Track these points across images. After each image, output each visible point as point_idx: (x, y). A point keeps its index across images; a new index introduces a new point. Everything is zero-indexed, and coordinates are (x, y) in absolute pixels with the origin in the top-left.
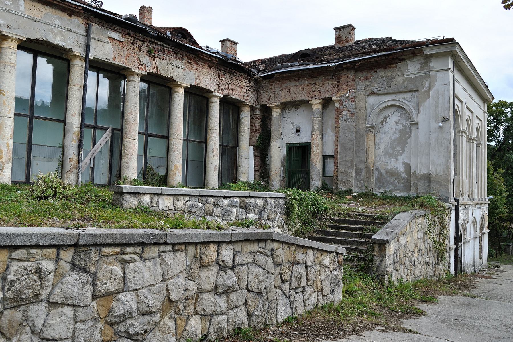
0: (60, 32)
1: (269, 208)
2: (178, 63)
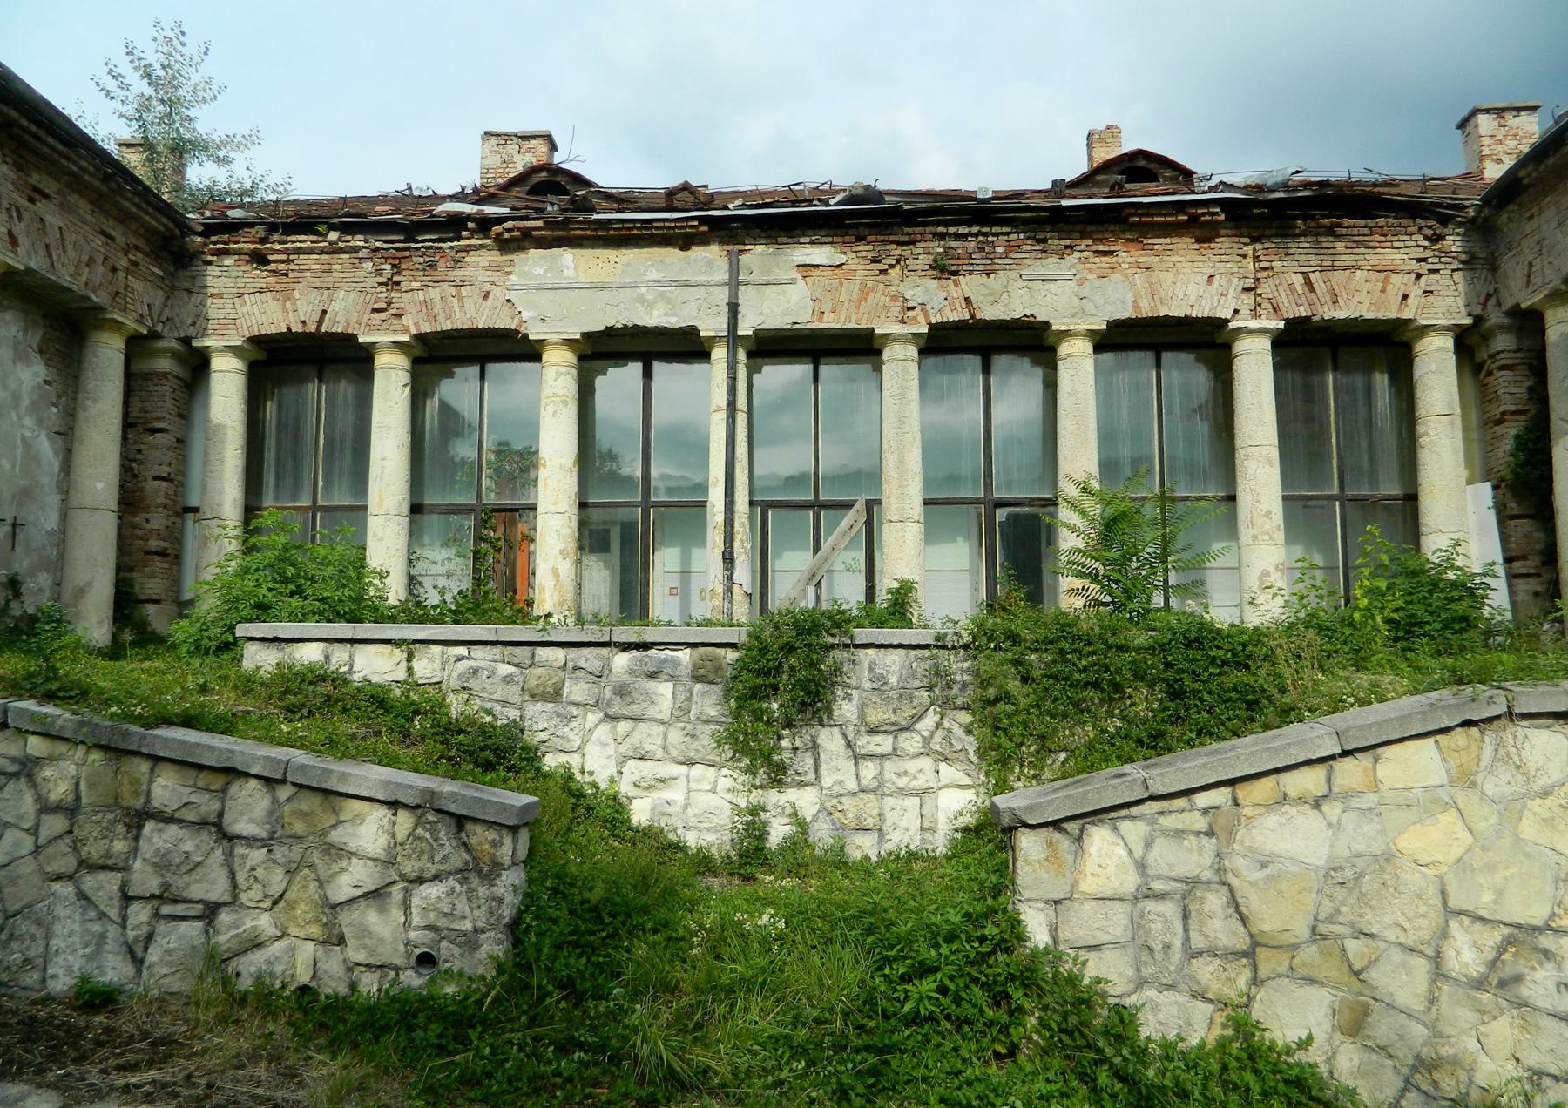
0: (662, 295)
1: (867, 685)
2: (1051, 266)
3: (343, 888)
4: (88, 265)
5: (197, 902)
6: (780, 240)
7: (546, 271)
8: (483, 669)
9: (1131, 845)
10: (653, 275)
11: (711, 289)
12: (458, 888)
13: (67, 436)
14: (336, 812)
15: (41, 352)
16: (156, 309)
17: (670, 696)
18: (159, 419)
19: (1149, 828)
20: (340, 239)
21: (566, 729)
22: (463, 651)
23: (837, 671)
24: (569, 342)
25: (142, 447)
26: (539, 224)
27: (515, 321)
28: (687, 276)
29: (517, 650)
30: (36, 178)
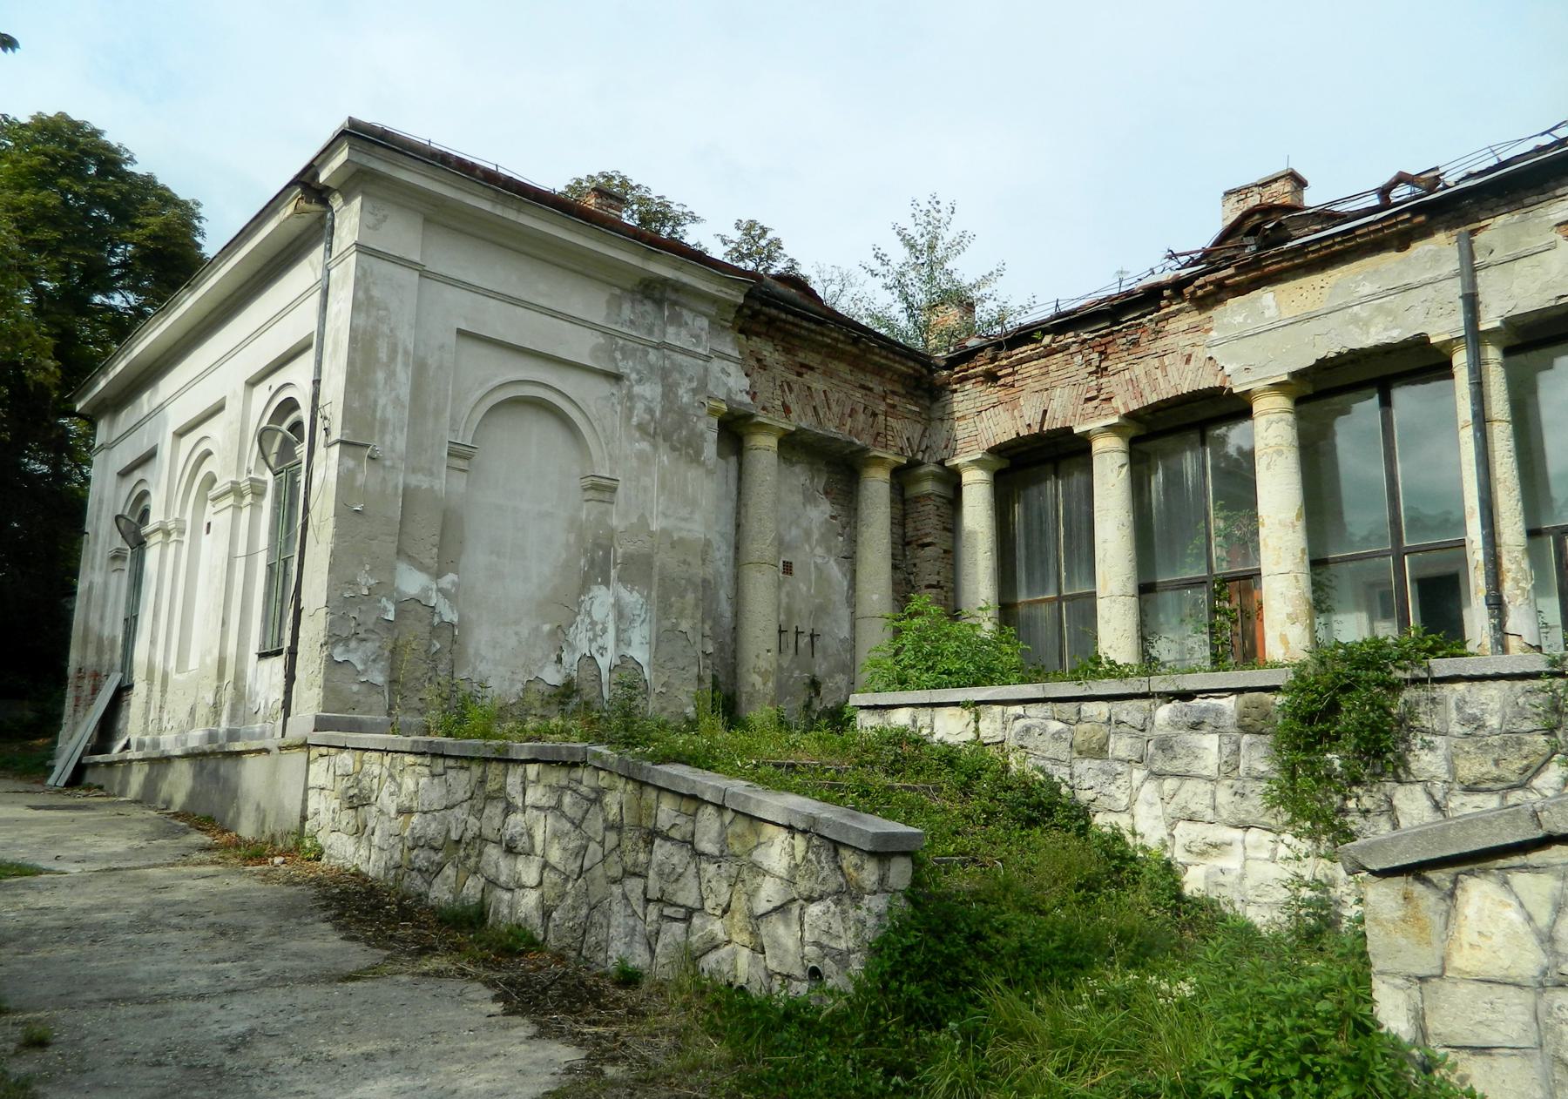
1: (1457, 729)
3: (762, 906)
4: (850, 416)
5: (682, 906)
6: (1527, 201)
7: (1246, 318)
8: (1035, 726)
9: (1530, 908)
10: (1367, 289)
11: (1440, 285)
12: (833, 908)
13: (850, 559)
14: (758, 834)
15: (826, 493)
16: (915, 442)
17: (1216, 749)
18: (927, 535)
19: (1559, 884)
20: (1053, 341)
21: (1113, 787)
22: (1018, 709)
23: (1411, 713)
24: (1278, 387)
25: (916, 561)
26: (1231, 271)
27: (1219, 377)
28: (1411, 279)
29: (1066, 706)
30: (802, 357)
